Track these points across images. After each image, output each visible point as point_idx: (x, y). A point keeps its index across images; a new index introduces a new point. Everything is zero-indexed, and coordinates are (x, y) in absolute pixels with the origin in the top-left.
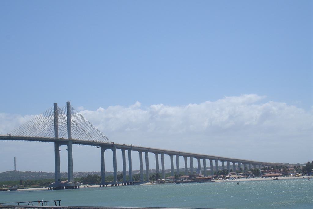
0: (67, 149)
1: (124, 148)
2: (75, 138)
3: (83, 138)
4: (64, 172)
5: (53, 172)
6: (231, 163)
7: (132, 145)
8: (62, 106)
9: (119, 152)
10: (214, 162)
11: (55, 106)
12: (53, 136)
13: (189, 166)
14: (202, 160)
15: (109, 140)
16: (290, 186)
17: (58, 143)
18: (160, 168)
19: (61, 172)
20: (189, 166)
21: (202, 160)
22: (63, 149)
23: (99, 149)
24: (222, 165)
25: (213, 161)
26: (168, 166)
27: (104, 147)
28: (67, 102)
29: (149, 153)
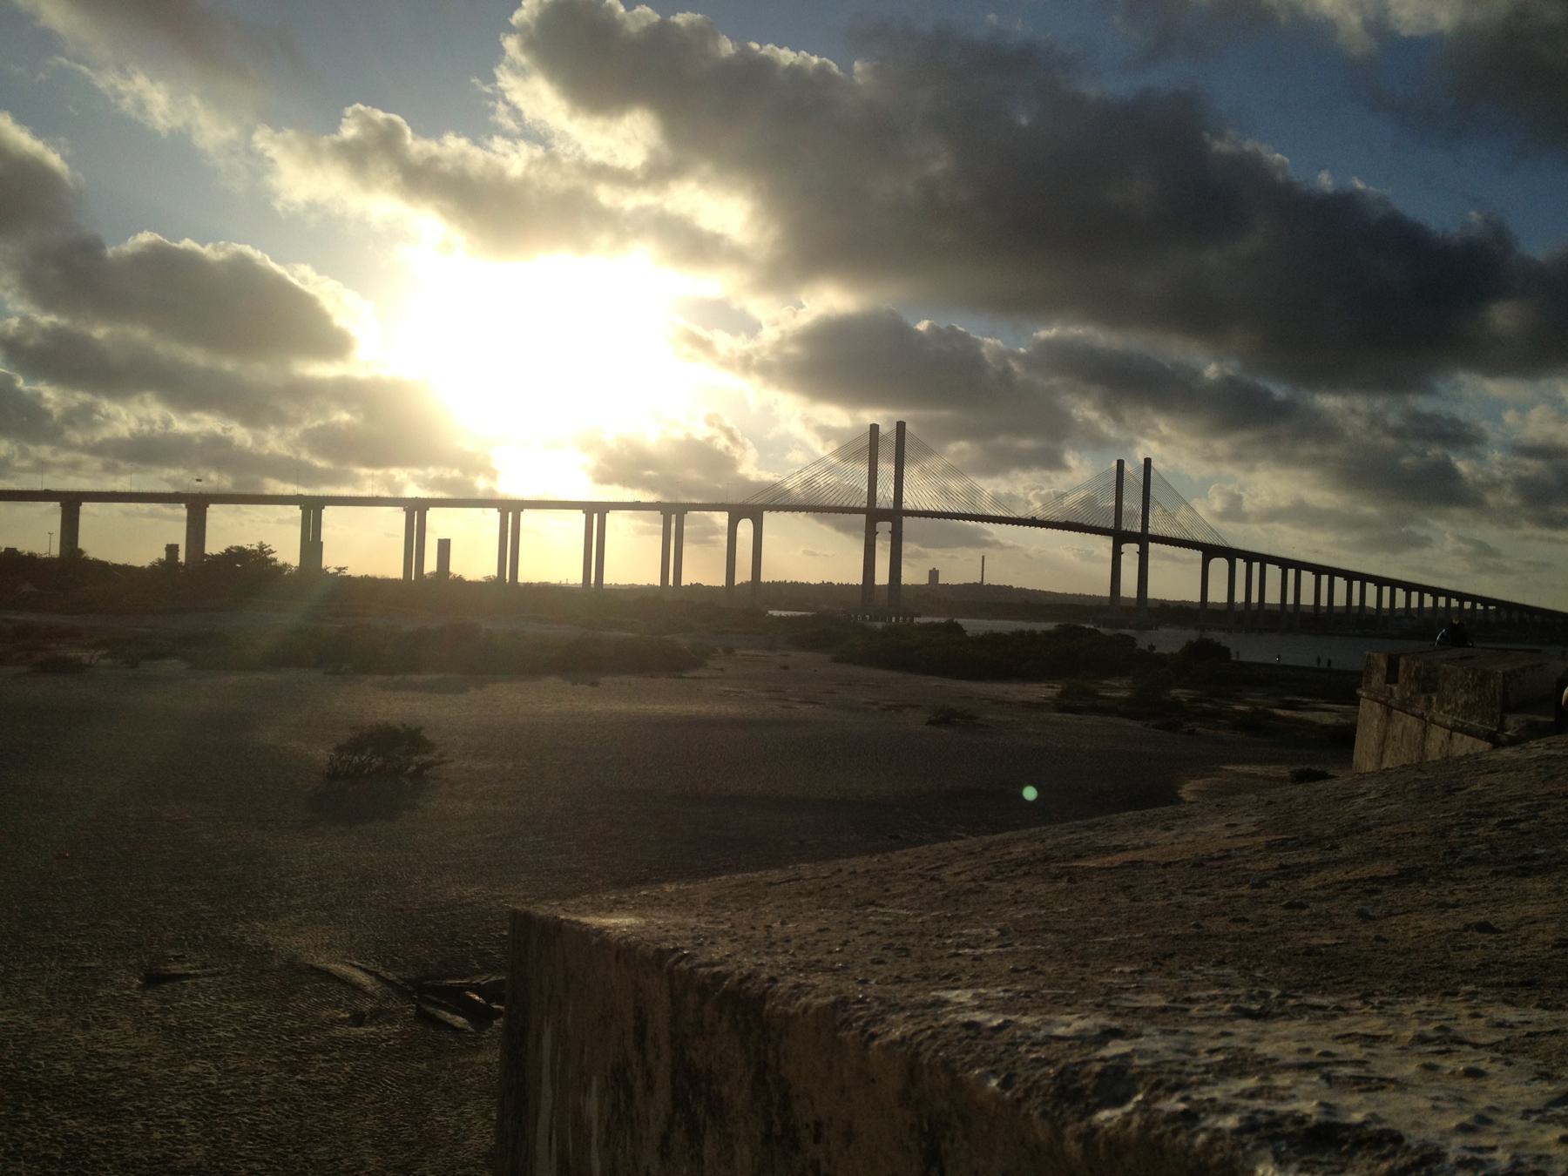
1: (1250, 557)
2: (947, 508)
5: (1195, 601)
6: (1479, 607)
8: (1133, 469)
9: (1241, 564)
11: (1120, 463)
12: (1111, 525)
13: (1356, 602)
14: (1356, 584)
15: (1223, 540)
17: (1120, 537)
18: (1290, 600)
20: (1356, 602)
21: (1356, 584)
23: (1198, 555)
24: (1108, 595)
26: (1307, 599)
27: (1210, 551)
28: (898, 423)
29: (1269, 567)
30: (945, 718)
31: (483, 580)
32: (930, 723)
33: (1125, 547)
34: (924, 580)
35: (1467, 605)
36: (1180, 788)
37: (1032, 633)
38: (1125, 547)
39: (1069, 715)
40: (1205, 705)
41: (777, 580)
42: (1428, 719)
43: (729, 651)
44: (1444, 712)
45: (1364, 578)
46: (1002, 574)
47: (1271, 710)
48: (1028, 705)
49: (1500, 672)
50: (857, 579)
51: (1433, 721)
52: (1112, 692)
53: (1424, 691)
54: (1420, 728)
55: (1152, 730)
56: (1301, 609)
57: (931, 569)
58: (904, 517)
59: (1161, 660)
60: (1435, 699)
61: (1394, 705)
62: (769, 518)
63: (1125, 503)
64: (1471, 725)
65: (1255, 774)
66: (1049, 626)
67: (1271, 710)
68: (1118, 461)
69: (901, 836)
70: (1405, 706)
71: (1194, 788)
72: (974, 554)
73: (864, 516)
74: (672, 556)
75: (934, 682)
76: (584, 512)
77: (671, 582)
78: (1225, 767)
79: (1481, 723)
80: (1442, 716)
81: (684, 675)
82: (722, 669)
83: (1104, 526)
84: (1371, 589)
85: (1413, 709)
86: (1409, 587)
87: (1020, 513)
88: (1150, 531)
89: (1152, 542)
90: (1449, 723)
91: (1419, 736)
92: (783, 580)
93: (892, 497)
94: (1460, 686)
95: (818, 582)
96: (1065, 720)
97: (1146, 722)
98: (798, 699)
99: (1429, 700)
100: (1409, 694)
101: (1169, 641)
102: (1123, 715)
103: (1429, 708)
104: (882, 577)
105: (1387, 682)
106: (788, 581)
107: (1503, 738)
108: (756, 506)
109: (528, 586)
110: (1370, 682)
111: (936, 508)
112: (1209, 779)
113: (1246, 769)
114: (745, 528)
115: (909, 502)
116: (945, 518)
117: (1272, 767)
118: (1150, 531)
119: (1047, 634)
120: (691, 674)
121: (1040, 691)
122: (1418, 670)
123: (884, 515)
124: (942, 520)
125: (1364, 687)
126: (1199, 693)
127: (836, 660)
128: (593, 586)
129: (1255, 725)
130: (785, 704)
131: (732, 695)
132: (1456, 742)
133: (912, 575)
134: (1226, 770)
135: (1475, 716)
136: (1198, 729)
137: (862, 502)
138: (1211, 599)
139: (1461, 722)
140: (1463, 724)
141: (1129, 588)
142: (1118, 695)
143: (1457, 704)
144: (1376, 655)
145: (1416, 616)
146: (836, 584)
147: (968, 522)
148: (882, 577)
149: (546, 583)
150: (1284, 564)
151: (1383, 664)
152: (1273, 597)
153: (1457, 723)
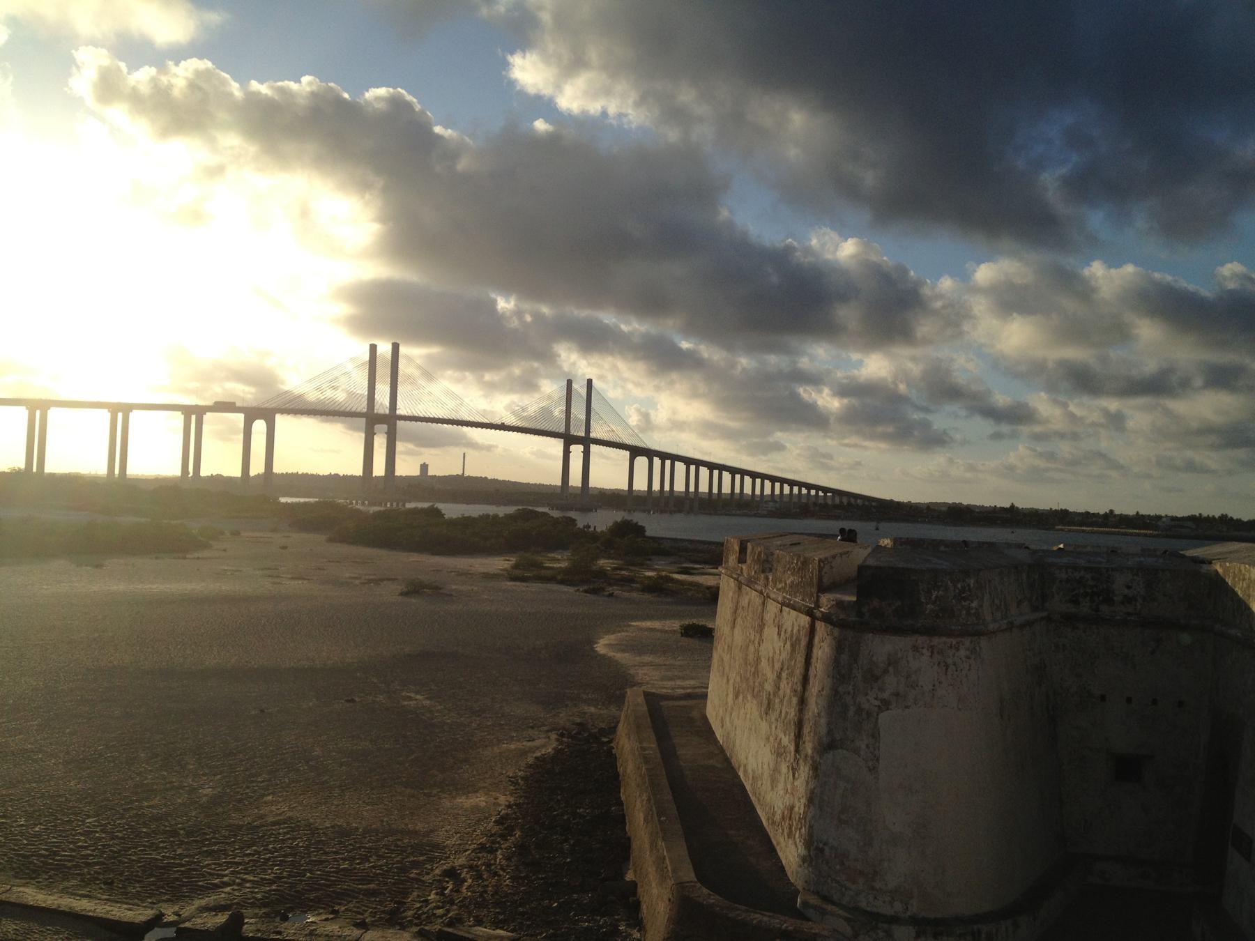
0: (1138, 513)
1: (664, 456)
2: (409, 411)
3: (408, 409)
4: (726, 492)
6: (821, 493)
7: (1138, 513)
8: (579, 388)
9: (657, 462)
10: (777, 485)
12: (562, 430)
14: (758, 481)
15: (644, 443)
16: (567, 706)
19: (590, 486)
21: (758, 481)
22: (577, 450)
24: (560, 484)
25: (776, 483)
26: (726, 489)
27: (635, 451)
29: (677, 463)
30: (415, 589)
31: (9, 471)
32: (402, 594)
33: (573, 448)
34: (415, 471)
35: (813, 492)
36: (597, 643)
37: (496, 517)
38: (573, 448)
39: (518, 583)
40: (623, 572)
41: (290, 472)
42: (765, 595)
43: (236, 533)
44: (777, 590)
45: (744, 473)
46: (478, 468)
47: (671, 575)
48: (487, 576)
49: (816, 559)
50: (357, 470)
51: (769, 597)
52: (555, 563)
53: (763, 571)
54: (761, 602)
55: (582, 594)
56: (723, 496)
57: (427, 463)
58: (398, 421)
59: (594, 537)
60: (771, 578)
61: (743, 581)
62: (280, 420)
63: (573, 410)
64: (795, 602)
65: (655, 628)
66: (511, 510)
67: (671, 575)
68: (568, 381)
69: (357, 699)
70: (751, 583)
71: (606, 642)
72: (457, 452)
73: (364, 420)
74: (192, 446)
75: (414, 558)
76: (182, 414)
77: (117, 471)
78: (632, 623)
79: (803, 600)
80: (774, 593)
81: (187, 556)
82: (225, 550)
83: (557, 431)
84: (768, 484)
85: (756, 586)
86: (773, 479)
87: (497, 421)
88: (592, 435)
89: (400, 420)
90: (780, 599)
91: (760, 608)
92: (295, 471)
93: (388, 405)
94: (789, 569)
95: (326, 473)
96: (514, 588)
97: (576, 588)
98: (289, 576)
99: (767, 579)
100: (753, 573)
101: (602, 521)
102: (562, 582)
103: (766, 586)
104: (379, 469)
105: (739, 562)
106: (300, 473)
107: (818, 614)
108: (269, 409)
109: (52, 475)
110: (728, 562)
111: (424, 413)
112: (619, 634)
113: (648, 624)
114: (259, 426)
115: (402, 410)
116: (457, 425)
117: (668, 622)
118: (592, 435)
119: (508, 517)
120: (196, 555)
121: (499, 564)
122: (760, 553)
123: (381, 419)
124: (434, 424)
125: (723, 565)
126: (620, 562)
127: (331, 540)
128: (116, 476)
129: (657, 588)
130: (278, 580)
131: (229, 573)
132: (785, 614)
133: (406, 467)
134: (634, 626)
135: (798, 595)
136: (616, 592)
137: (362, 406)
138: (636, 487)
139: (788, 599)
140: (790, 600)
141: (575, 479)
142: (558, 565)
143: (786, 584)
144: (732, 540)
145: (778, 500)
146: (342, 475)
147: (445, 425)
148: (379, 469)
149: (77, 473)
150: (688, 461)
151: (737, 548)
152: (704, 488)
153: (785, 600)
